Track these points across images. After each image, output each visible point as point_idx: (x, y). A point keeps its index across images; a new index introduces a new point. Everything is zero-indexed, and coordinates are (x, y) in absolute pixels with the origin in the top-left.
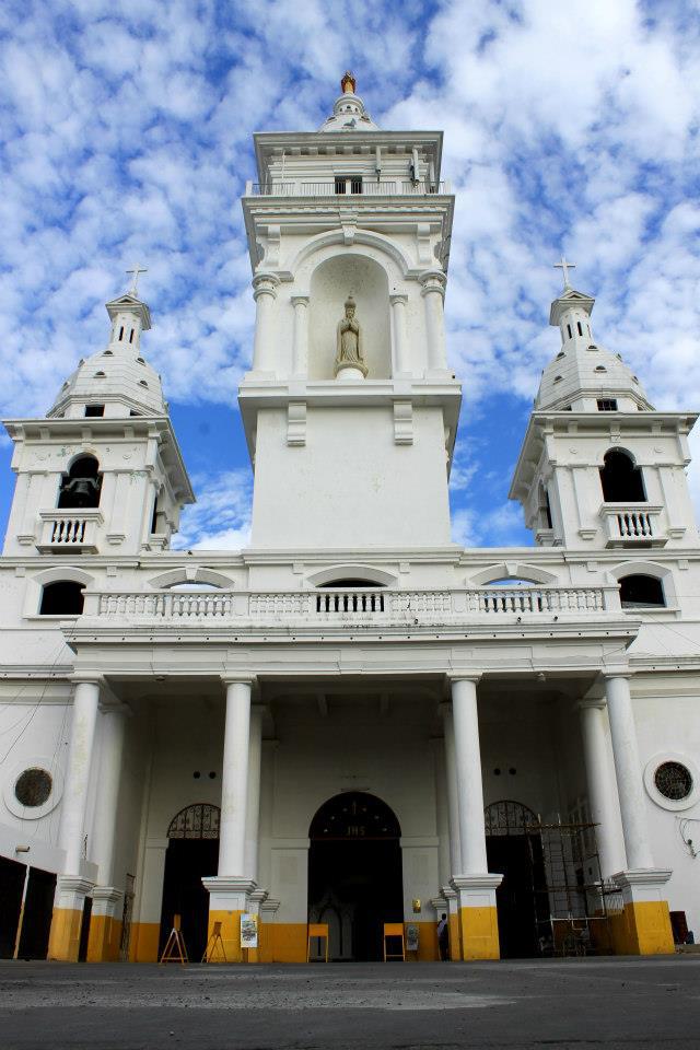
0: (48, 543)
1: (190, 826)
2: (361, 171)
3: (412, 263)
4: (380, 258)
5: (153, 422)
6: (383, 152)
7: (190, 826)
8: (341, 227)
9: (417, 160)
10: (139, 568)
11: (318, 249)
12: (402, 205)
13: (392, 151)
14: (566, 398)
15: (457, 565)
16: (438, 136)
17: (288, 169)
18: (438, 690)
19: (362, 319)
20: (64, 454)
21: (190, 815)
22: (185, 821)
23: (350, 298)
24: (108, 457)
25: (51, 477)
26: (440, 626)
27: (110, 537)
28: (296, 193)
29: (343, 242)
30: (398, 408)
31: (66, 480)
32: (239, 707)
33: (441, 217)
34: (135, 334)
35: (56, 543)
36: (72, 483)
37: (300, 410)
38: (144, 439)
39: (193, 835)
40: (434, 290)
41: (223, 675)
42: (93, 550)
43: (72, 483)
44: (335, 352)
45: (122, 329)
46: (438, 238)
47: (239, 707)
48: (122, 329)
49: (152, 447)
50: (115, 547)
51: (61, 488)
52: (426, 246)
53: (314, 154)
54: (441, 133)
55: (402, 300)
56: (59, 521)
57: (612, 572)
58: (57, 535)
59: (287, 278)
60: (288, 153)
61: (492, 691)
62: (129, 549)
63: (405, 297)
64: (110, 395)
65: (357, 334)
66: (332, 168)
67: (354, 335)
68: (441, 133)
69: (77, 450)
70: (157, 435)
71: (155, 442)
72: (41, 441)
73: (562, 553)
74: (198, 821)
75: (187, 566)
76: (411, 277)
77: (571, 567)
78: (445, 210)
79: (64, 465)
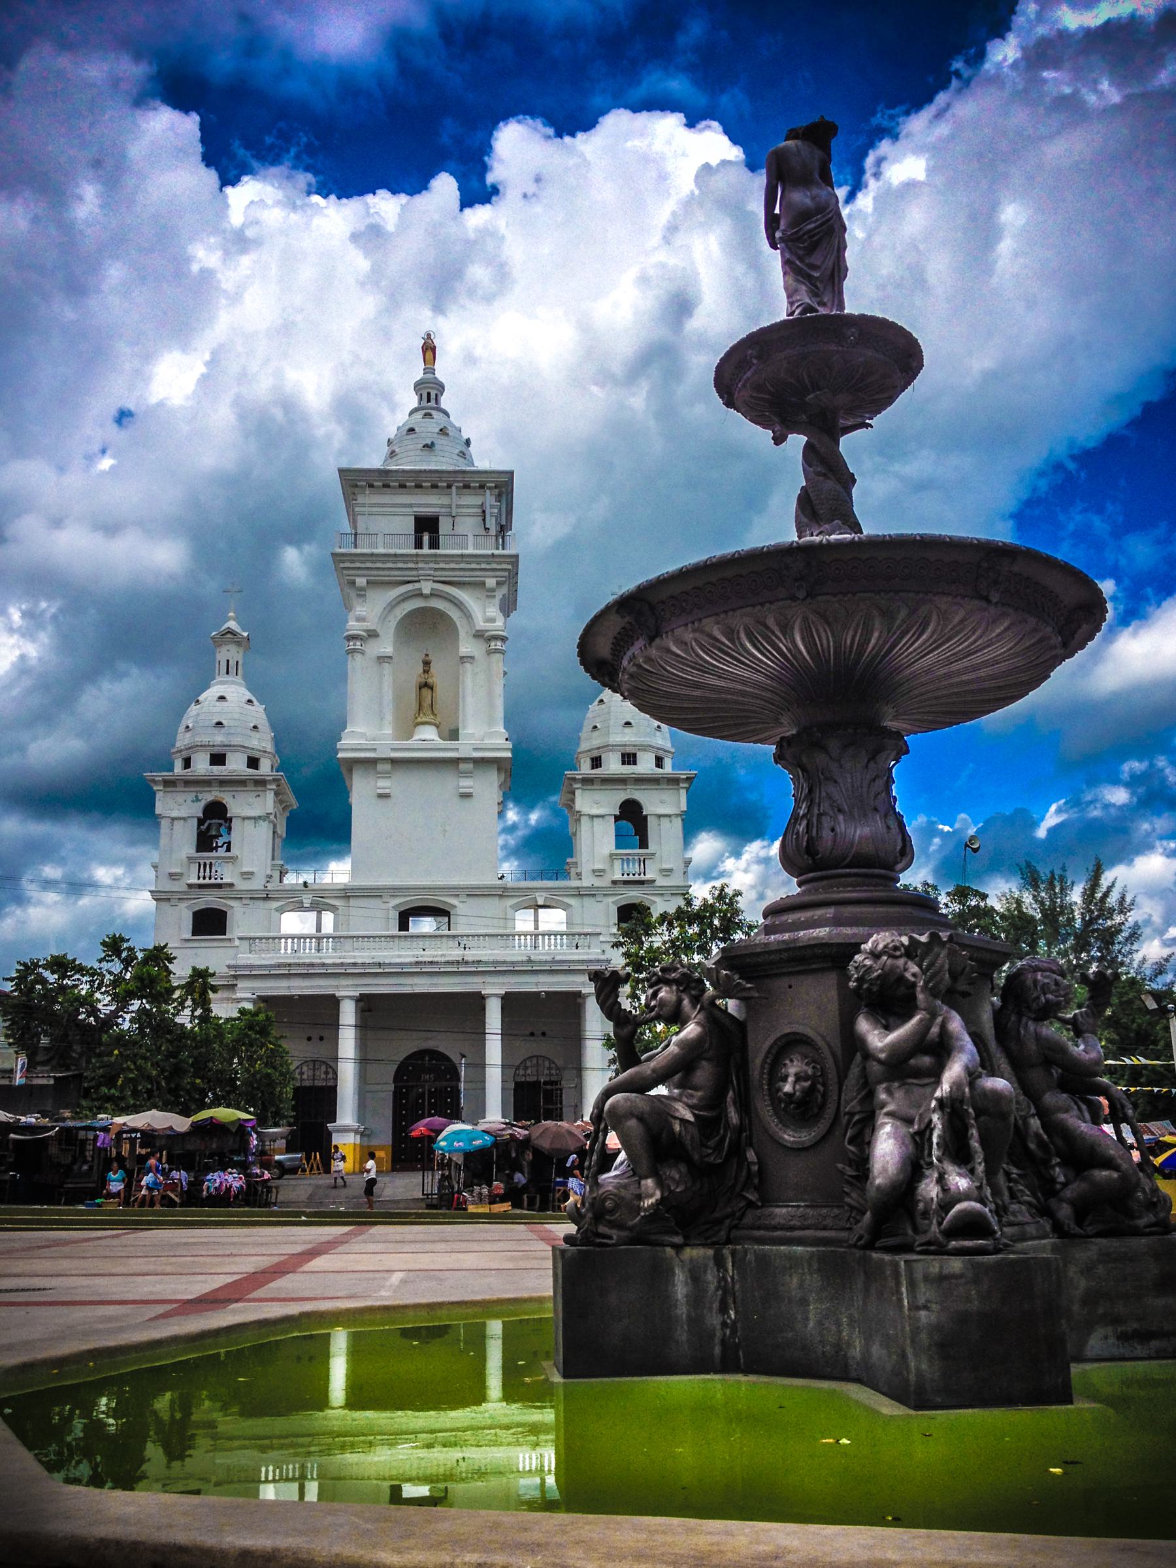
0: (194, 880)
1: (305, 1077)
2: (437, 510)
3: (480, 624)
4: (454, 614)
5: (271, 778)
6: (458, 488)
7: (305, 1077)
8: (419, 581)
9: (489, 499)
10: (267, 898)
11: (403, 600)
12: (473, 562)
13: (467, 487)
14: (598, 748)
15: (500, 896)
16: (510, 476)
17: (372, 506)
18: (477, 1001)
19: (437, 677)
20: (197, 800)
21: (305, 1069)
22: (301, 1073)
23: (427, 655)
24: (239, 805)
25: (190, 821)
26: (479, 962)
27: (243, 874)
28: (381, 550)
29: (419, 594)
30: (462, 766)
31: (201, 822)
32: (348, 1014)
33: (506, 574)
34: (240, 663)
35: (201, 881)
36: (206, 824)
37: (388, 767)
38: (263, 789)
39: (307, 1084)
40: (497, 651)
41: (338, 994)
42: (231, 885)
43: (206, 824)
44: (414, 706)
45: (228, 661)
46: (504, 590)
47: (348, 1014)
48: (228, 661)
49: (270, 796)
50: (245, 882)
51: (198, 828)
52: (491, 600)
53: (394, 487)
54: (512, 473)
55: (469, 660)
56: (202, 862)
57: (613, 903)
58: (202, 874)
59: (373, 634)
60: (371, 486)
61: (510, 1002)
62: (257, 884)
63: (472, 658)
64: (230, 746)
65: (432, 689)
66: (411, 506)
67: (430, 691)
68: (512, 473)
69: (209, 796)
70: (274, 787)
71: (273, 792)
72: (178, 789)
73: (578, 888)
74: (311, 1073)
75: (304, 896)
76: (479, 635)
77: (586, 899)
78: (510, 567)
79: (197, 810)
